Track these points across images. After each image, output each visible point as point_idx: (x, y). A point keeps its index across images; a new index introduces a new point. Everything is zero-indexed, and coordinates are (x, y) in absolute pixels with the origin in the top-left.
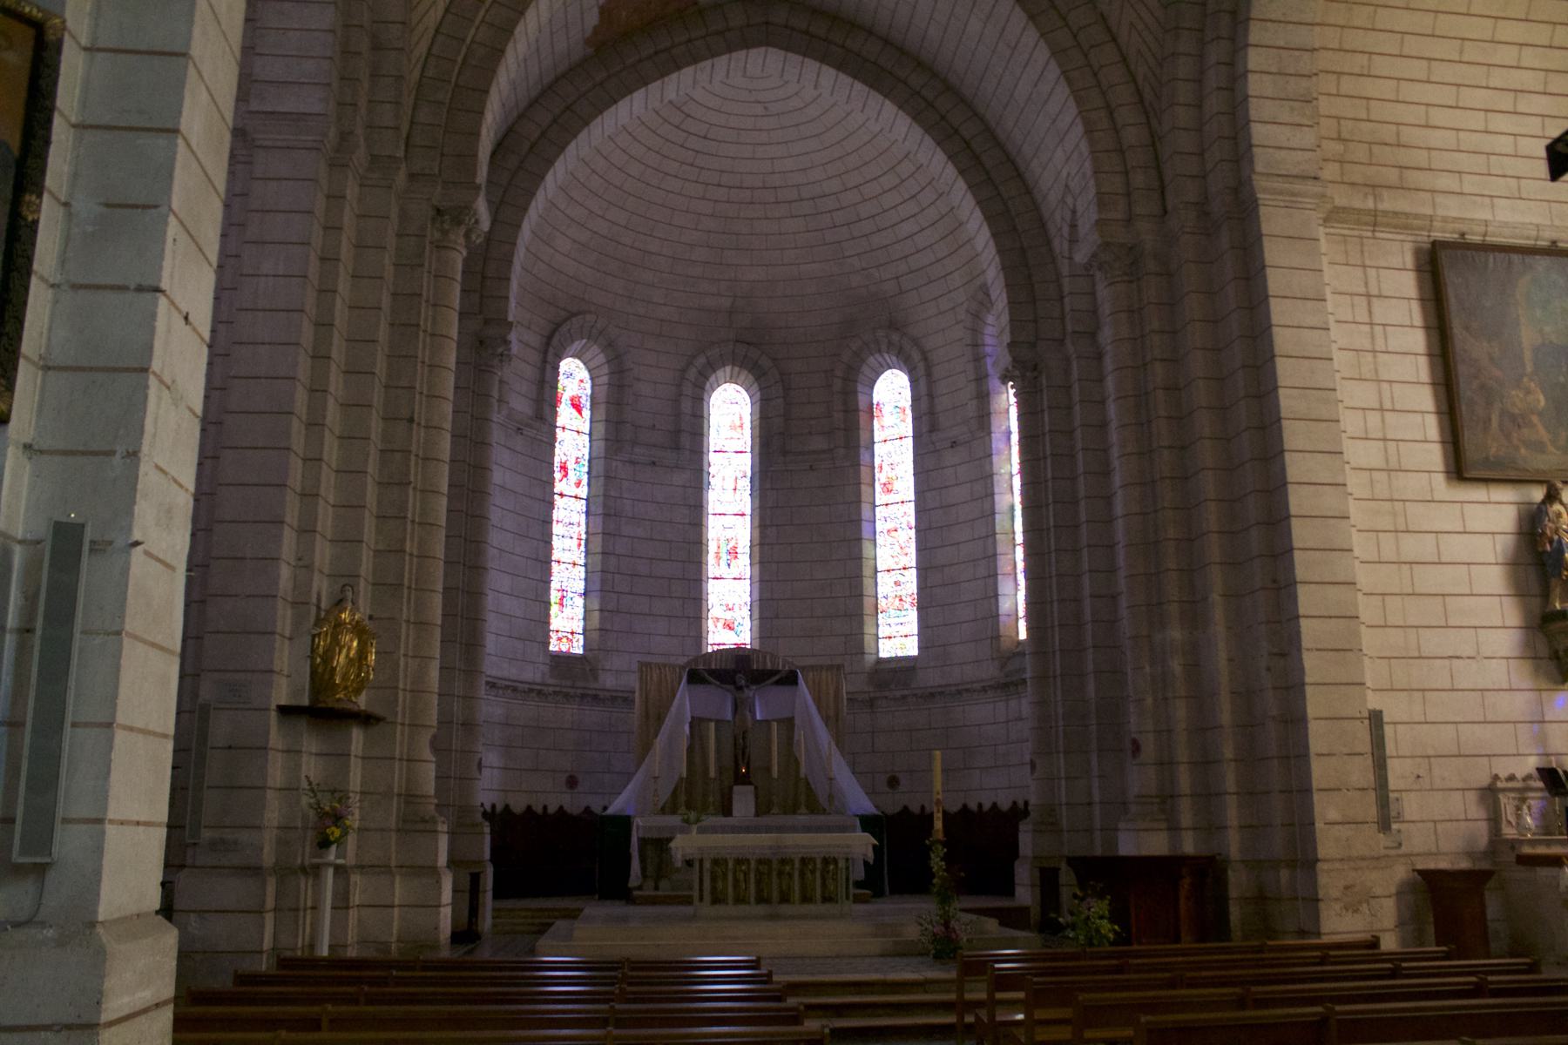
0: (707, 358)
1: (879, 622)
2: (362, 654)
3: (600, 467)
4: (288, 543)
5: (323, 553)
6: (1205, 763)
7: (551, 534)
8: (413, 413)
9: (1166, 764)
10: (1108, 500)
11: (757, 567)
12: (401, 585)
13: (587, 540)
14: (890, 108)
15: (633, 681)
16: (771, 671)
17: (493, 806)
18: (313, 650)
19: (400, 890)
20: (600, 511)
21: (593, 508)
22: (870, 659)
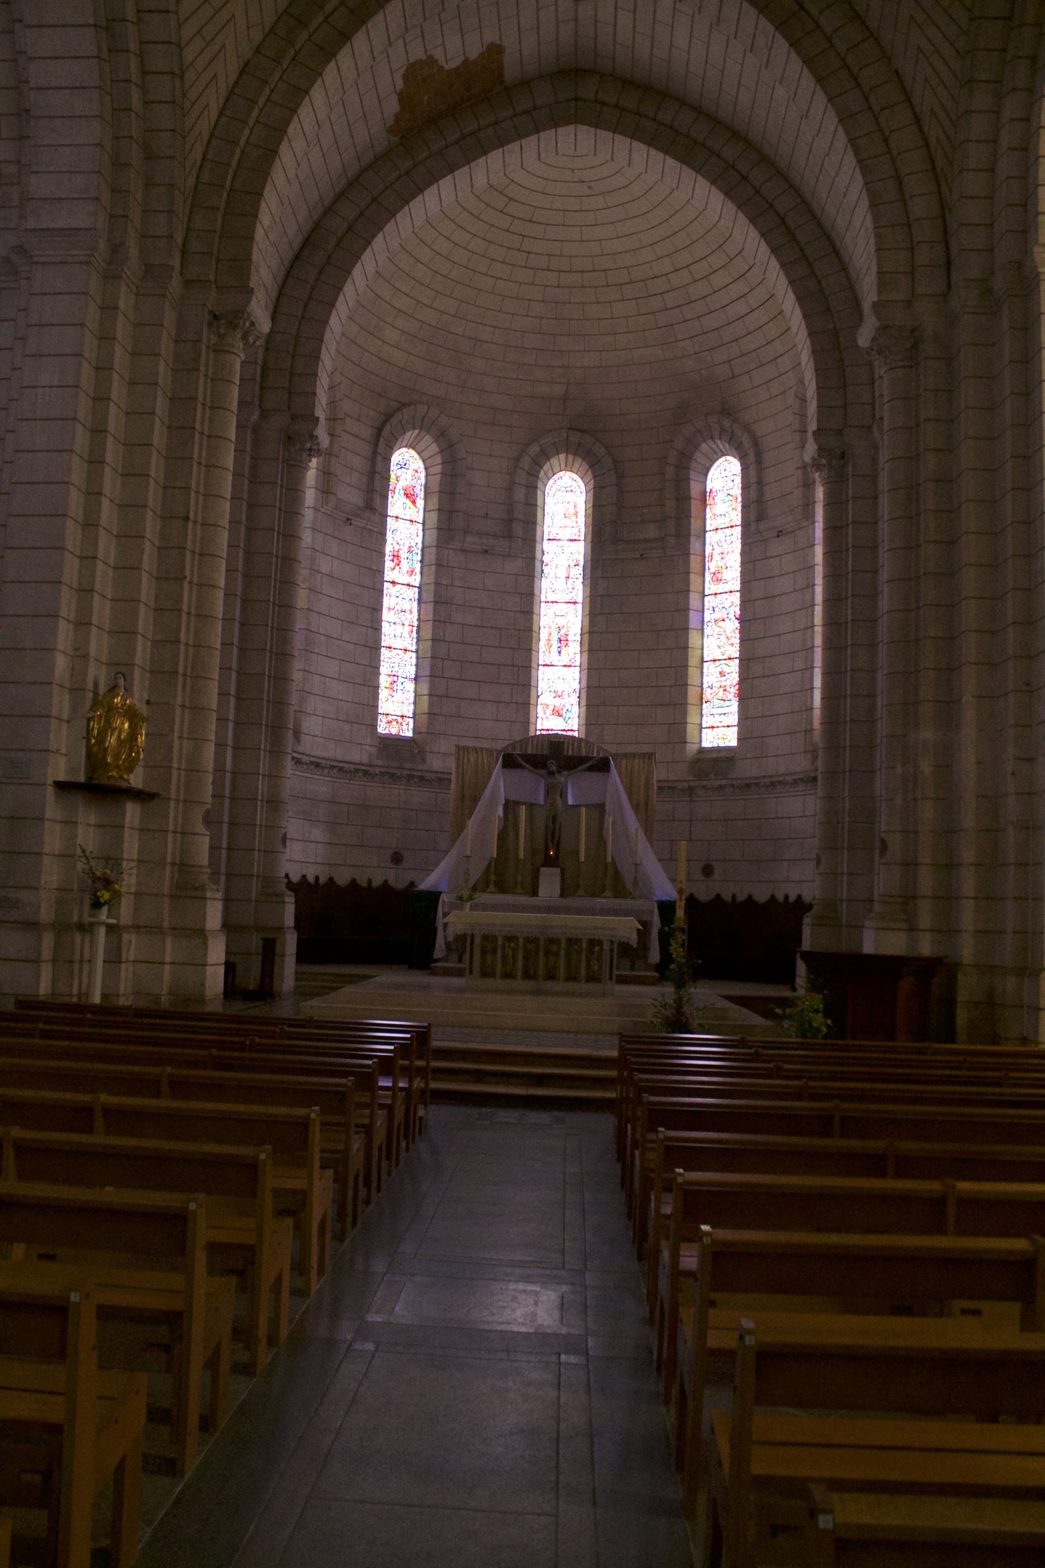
0: (541, 446)
1: (704, 712)
2: (133, 736)
3: (432, 557)
4: (64, 635)
5: (98, 644)
6: (949, 867)
7: (380, 621)
8: (188, 512)
9: (911, 865)
10: (873, 595)
11: (586, 655)
12: (176, 672)
13: (418, 627)
14: (702, 184)
15: (451, 764)
16: (572, 758)
17: (317, 878)
18: (89, 731)
19: (170, 949)
20: (431, 598)
21: (424, 595)
22: (691, 749)
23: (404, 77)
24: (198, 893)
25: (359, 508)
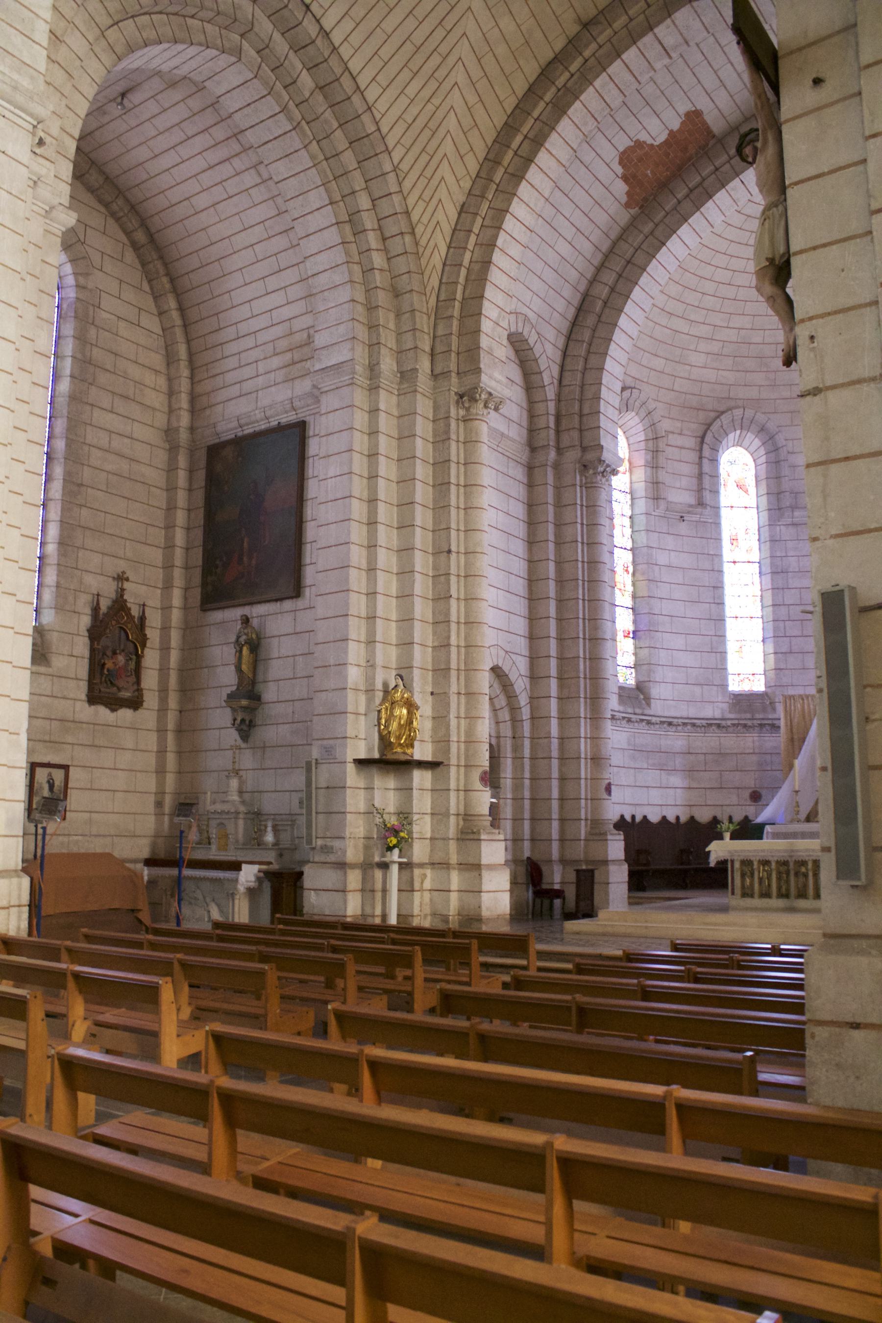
3: (766, 532)
17: (678, 818)
19: (455, 880)
21: (763, 569)
23: (620, 163)
24: (476, 837)
25: (691, 506)
